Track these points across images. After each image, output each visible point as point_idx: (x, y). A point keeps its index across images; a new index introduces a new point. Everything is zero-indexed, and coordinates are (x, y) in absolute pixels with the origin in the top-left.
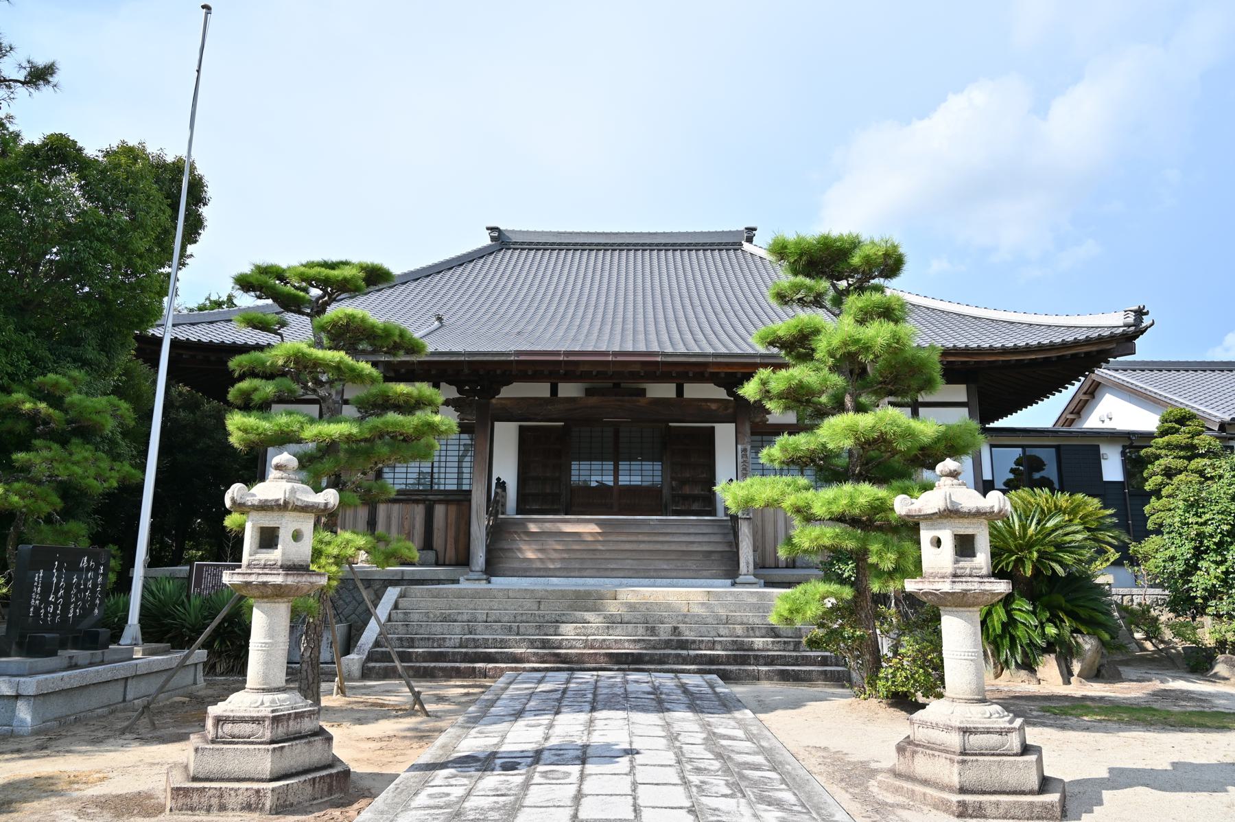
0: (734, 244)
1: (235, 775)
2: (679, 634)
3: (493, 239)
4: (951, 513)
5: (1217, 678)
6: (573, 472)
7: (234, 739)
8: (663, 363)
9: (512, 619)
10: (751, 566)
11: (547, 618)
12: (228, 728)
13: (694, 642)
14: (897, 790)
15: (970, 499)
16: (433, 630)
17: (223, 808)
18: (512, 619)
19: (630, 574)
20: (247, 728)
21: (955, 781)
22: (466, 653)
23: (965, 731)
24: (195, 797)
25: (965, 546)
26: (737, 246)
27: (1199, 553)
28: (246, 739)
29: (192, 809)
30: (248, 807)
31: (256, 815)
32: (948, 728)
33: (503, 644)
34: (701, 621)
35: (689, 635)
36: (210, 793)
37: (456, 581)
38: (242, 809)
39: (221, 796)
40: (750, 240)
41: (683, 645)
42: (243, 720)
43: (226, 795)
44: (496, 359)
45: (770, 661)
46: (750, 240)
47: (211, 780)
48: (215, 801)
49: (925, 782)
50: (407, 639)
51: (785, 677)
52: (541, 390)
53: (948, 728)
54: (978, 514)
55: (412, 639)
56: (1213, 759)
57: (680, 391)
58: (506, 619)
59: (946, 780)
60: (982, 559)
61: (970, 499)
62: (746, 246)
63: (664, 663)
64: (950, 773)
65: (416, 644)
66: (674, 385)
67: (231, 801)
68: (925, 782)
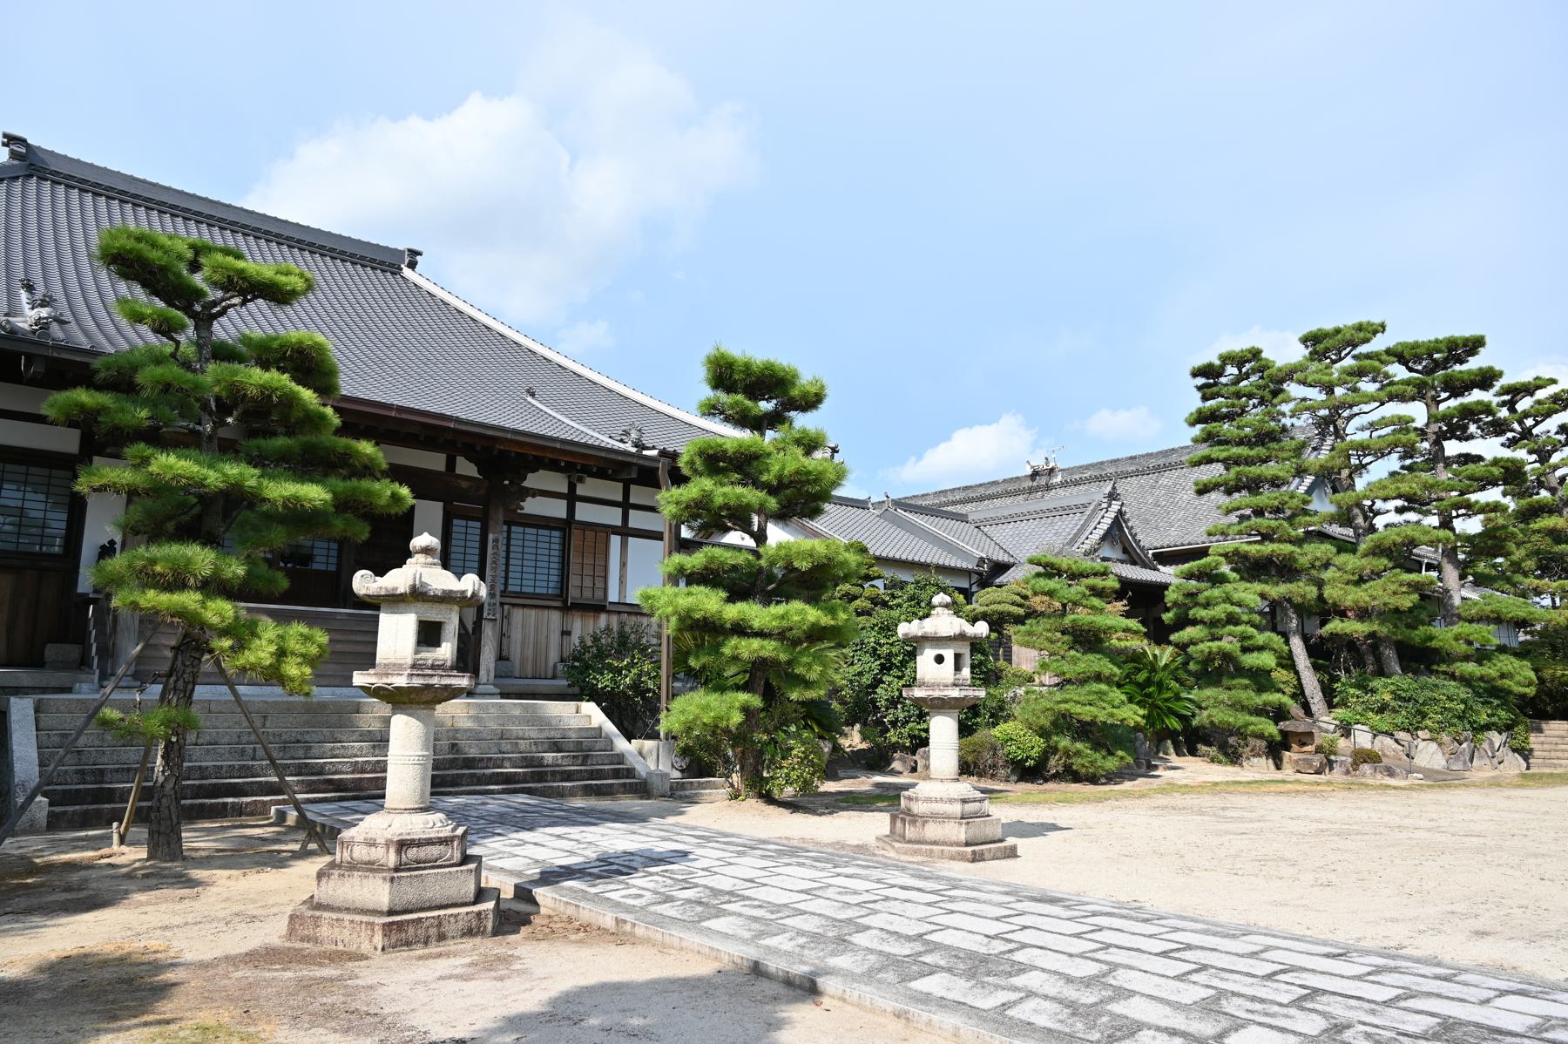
0: (391, 265)
1: (437, 902)
2: (458, 752)
3: (13, 155)
4: (418, 595)
5: (894, 773)
6: (555, 579)
7: (420, 864)
8: (455, 431)
9: (235, 739)
10: (492, 675)
11: (284, 737)
12: (412, 853)
13: (482, 760)
14: (915, 852)
15: (441, 580)
16: (124, 758)
17: (442, 937)
18: (235, 739)
19: (337, 681)
20: (434, 851)
21: (963, 837)
22: (200, 786)
23: (964, 801)
24: (411, 930)
25: (429, 634)
26: (395, 270)
27: (885, 669)
28: (433, 863)
29: (408, 944)
30: (470, 933)
31: (478, 940)
32: (951, 801)
33: (246, 771)
34: (475, 736)
35: (473, 752)
36: (427, 923)
37: (69, 690)
38: (463, 935)
39: (440, 925)
40: (412, 265)
41: (470, 763)
42: (430, 842)
43: (445, 923)
44: (65, 356)
45: (568, 776)
46: (412, 265)
47: (411, 912)
48: (433, 931)
49: (935, 843)
50: (93, 771)
51: (589, 791)
53: (951, 801)
54: (447, 598)
55: (102, 772)
56: (1031, 821)
58: (226, 739)
59: (954, 839)
60: (446, 651)
61: (441, 580)
62: (407, 272)
63: (457, 785)
64: (959, 832)
65: (108, 777)
66: (444, 456)
67: (450, 928)
68: (935, 843)
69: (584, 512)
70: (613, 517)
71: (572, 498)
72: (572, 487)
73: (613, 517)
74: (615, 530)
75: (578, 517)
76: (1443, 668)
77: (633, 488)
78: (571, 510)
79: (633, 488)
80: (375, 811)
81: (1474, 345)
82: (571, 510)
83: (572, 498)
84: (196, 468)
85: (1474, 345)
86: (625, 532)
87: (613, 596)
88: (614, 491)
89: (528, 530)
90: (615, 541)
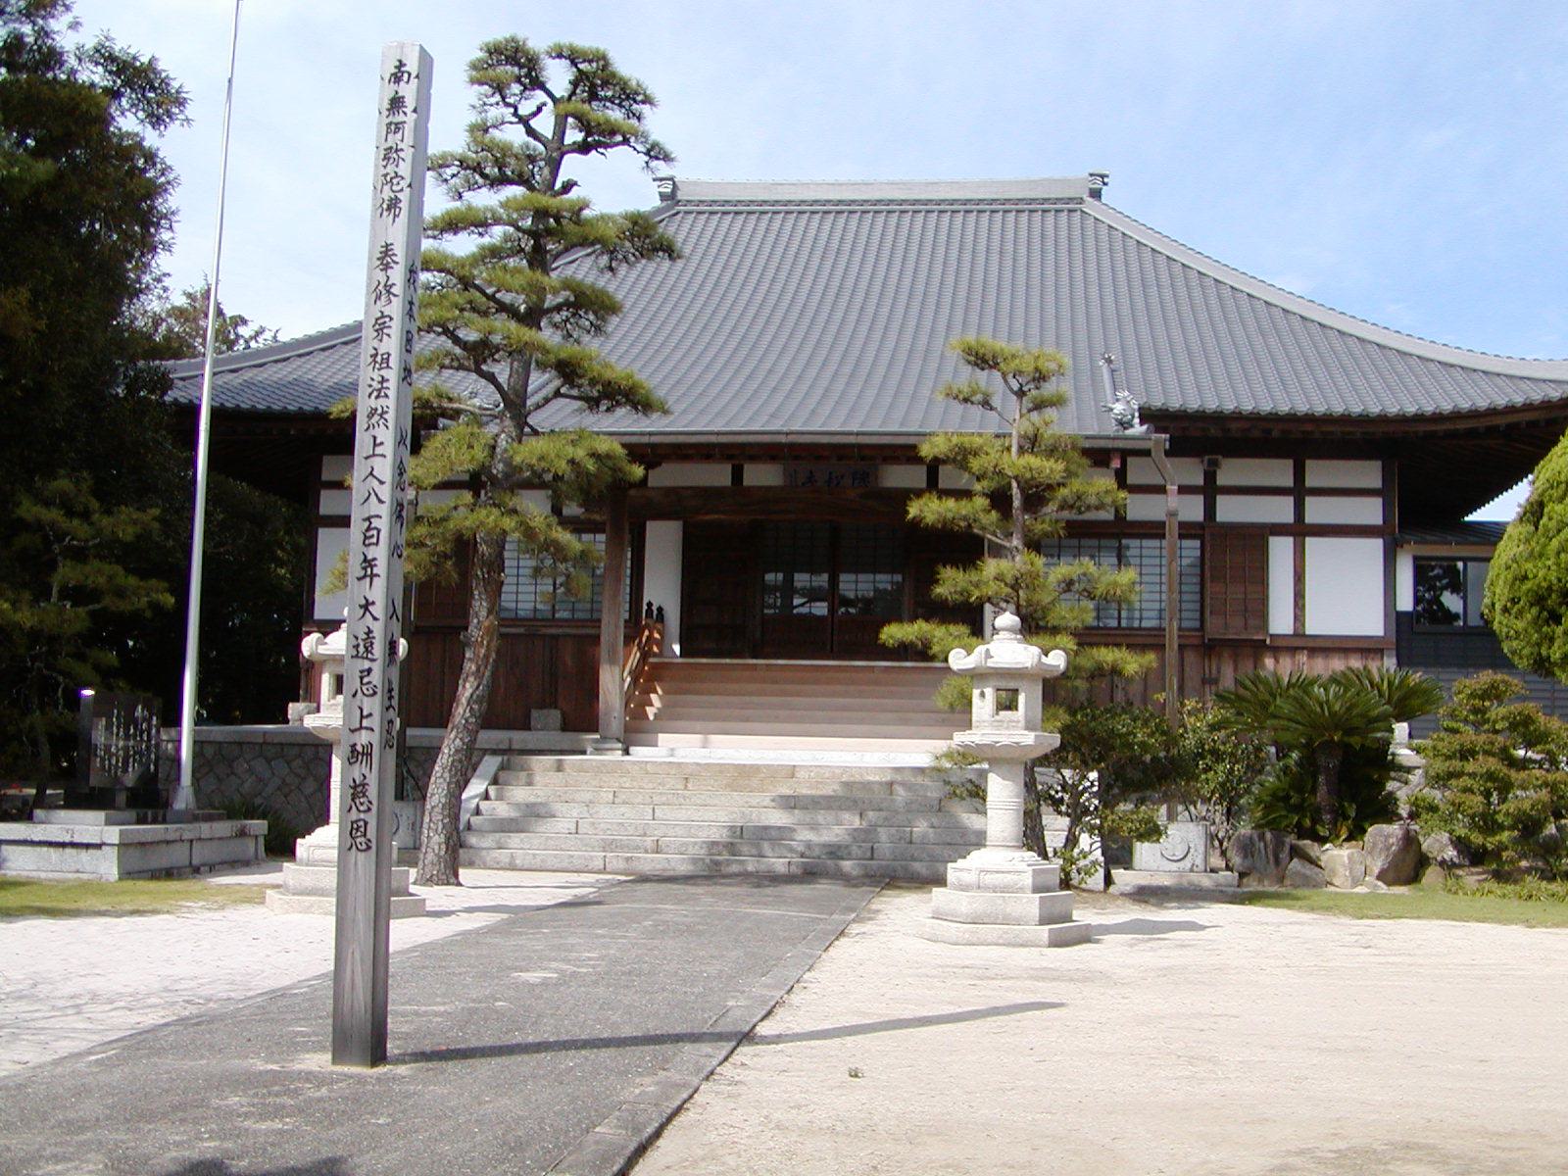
25: (1007, 704)
52: (718, 475)
57: (737, 475)
69: (1232, 510)
70: (1281, 510)
71: (1210, 491)
72: (1210, 476)
73: (1281, 510)
74: (1279, 530)
75: (1288, 465)
76: (498, 232)
77: (1309, 464)
78: (1210, 509)
79: (1309, 464)
80: (1484, 544)
81: (648, 100)
82: (1210, 509)
83: (1210, 491)
84: (906, 598)
85: (648, 100)
86: (1300, 530)
87: (1280, 622)
88: (1280, 472)
89: (1146, 543)
90: (1281, 550)
